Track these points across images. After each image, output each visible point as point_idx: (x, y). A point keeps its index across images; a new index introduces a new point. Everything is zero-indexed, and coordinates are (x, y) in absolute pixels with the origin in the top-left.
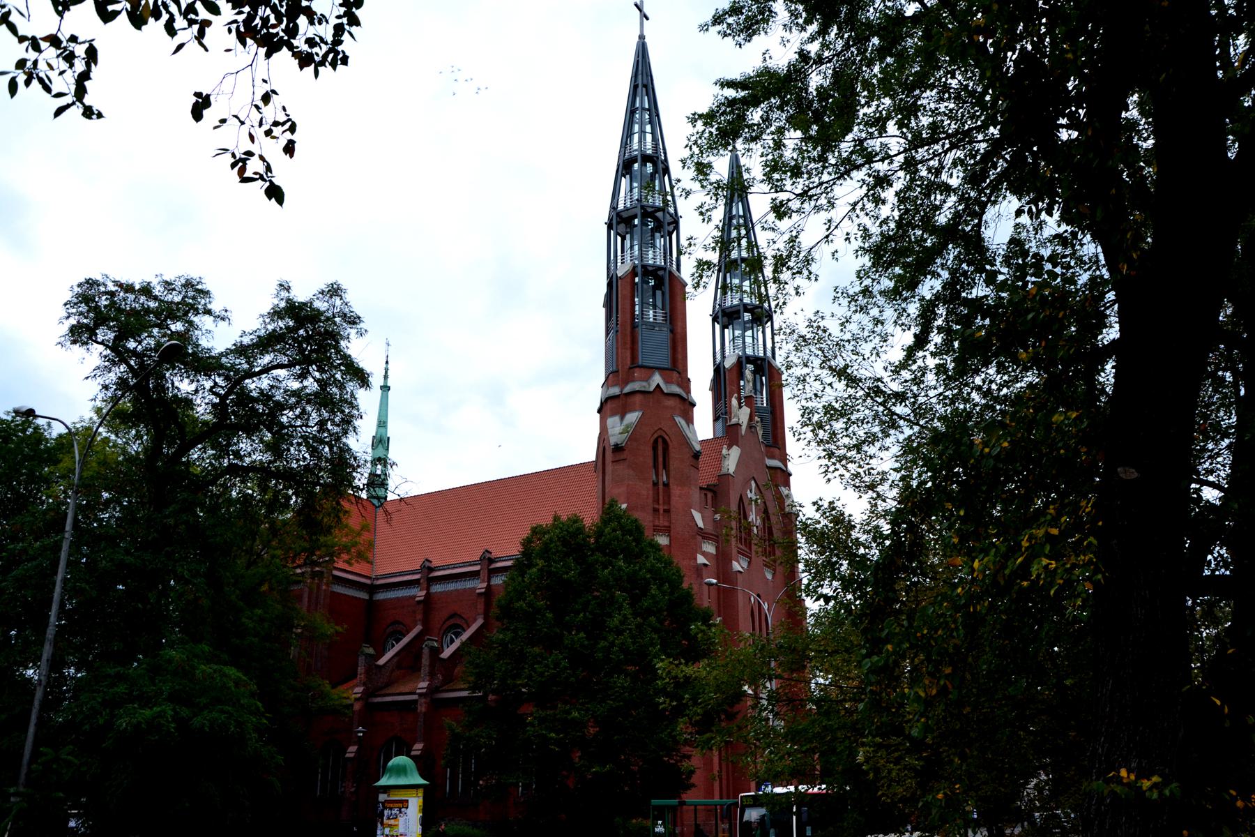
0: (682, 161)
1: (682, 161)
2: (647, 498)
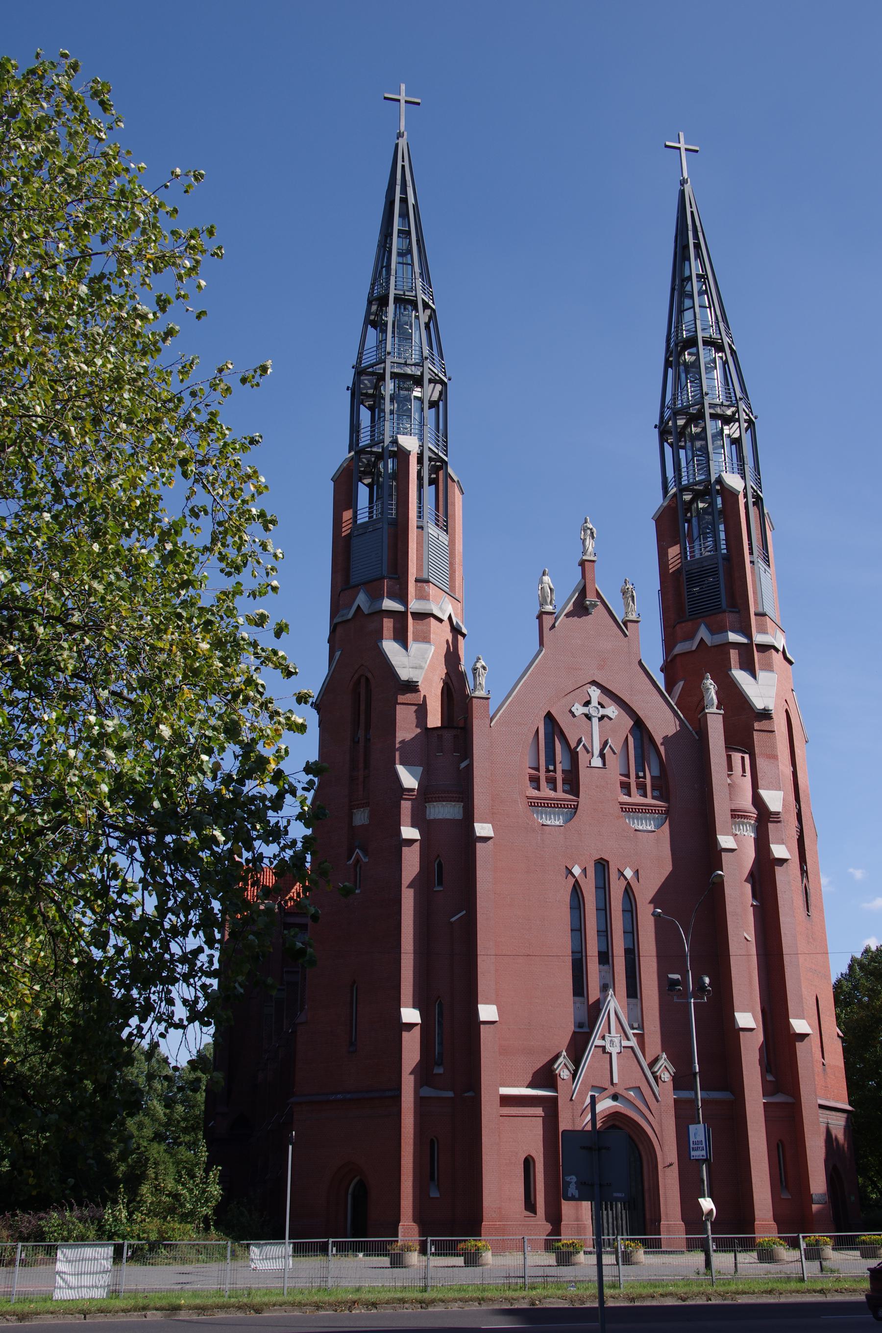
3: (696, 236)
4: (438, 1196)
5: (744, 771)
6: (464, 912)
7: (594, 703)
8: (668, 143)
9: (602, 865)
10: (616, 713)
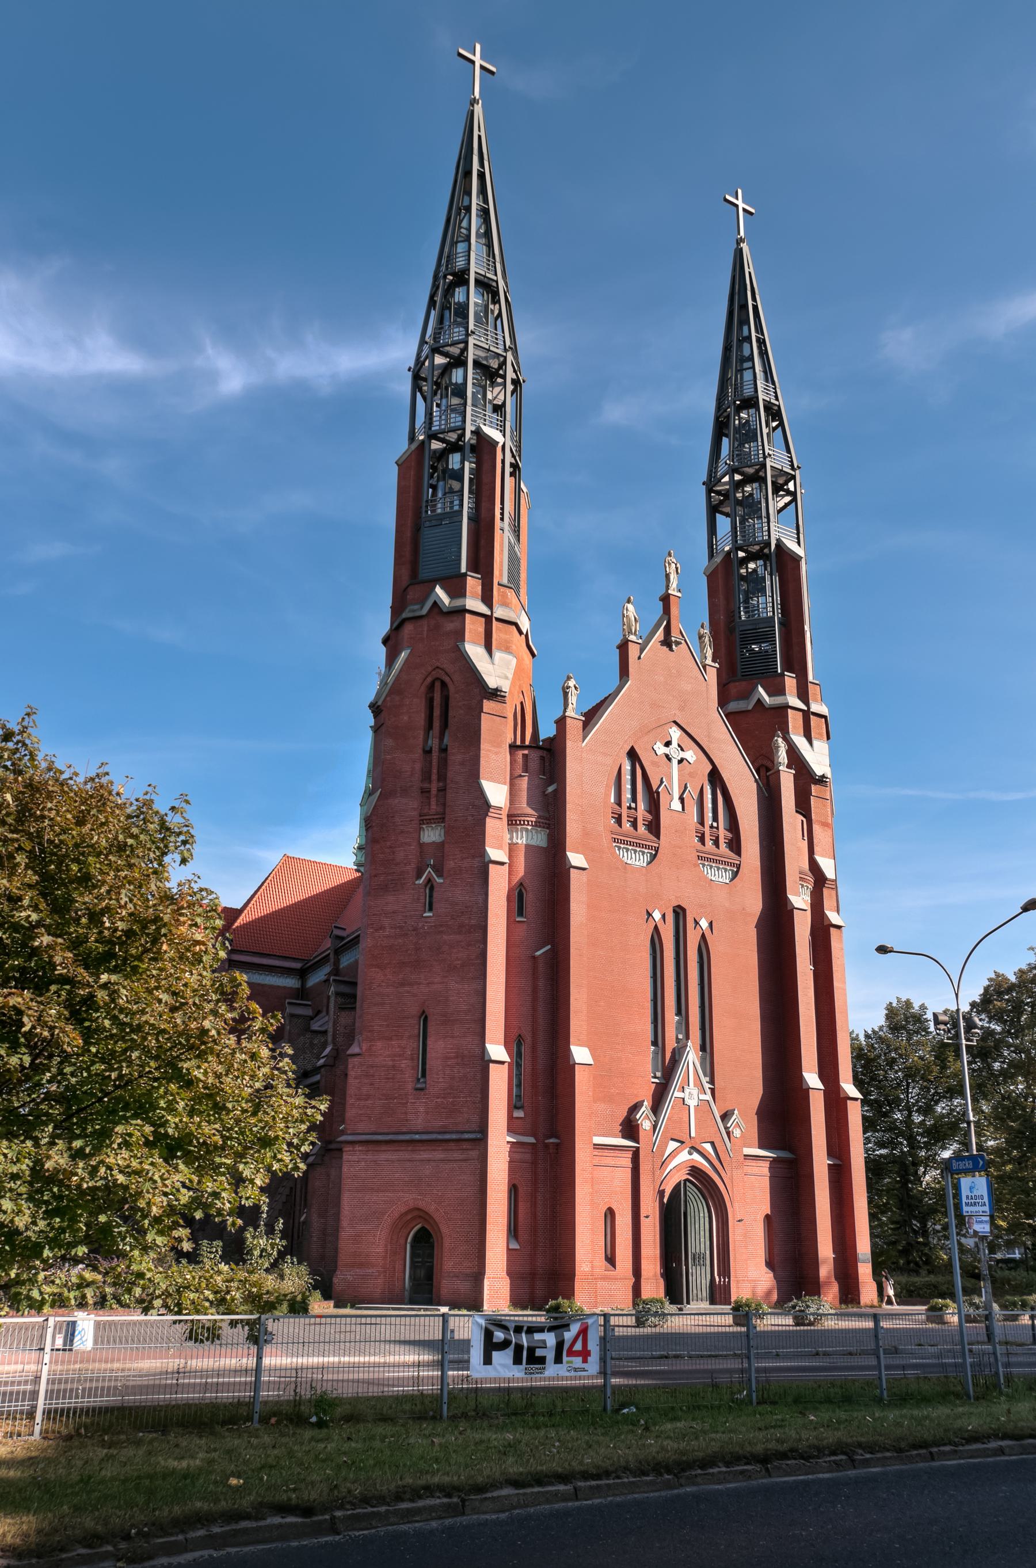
3: (754, 299)
4: (518, 1247)
5: (803, 836)
6: (549, 947)
7: (675, 744)
8: (728, 197)
9: (679, 912)
10: (695, 758)
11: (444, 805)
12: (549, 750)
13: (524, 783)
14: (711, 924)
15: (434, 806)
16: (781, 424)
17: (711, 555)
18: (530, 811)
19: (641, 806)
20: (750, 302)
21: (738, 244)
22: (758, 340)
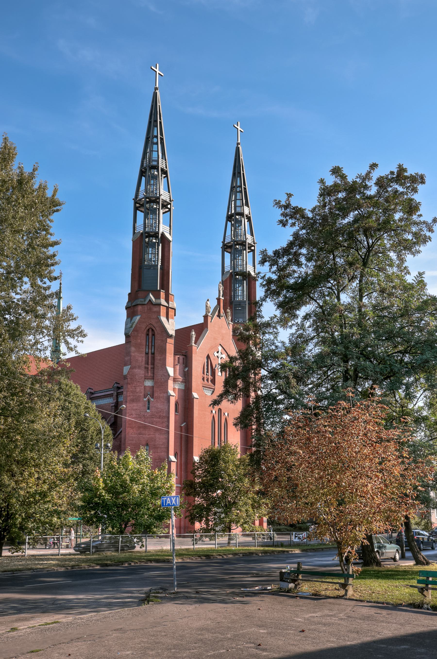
0: (288, 194)
1: (288, 194)
2: (142, 362)
8: (152, 67)
11: (154, 373)
12: (185, 356)
13: (178, 367)
14: (228, 414)
15: (149, 374)
16: (167, 176)
17: (134, 233)
18: (180, 377)
19: (210, 373)
20: (159, 120)
21: (155, 90)
22: (161, 138)
